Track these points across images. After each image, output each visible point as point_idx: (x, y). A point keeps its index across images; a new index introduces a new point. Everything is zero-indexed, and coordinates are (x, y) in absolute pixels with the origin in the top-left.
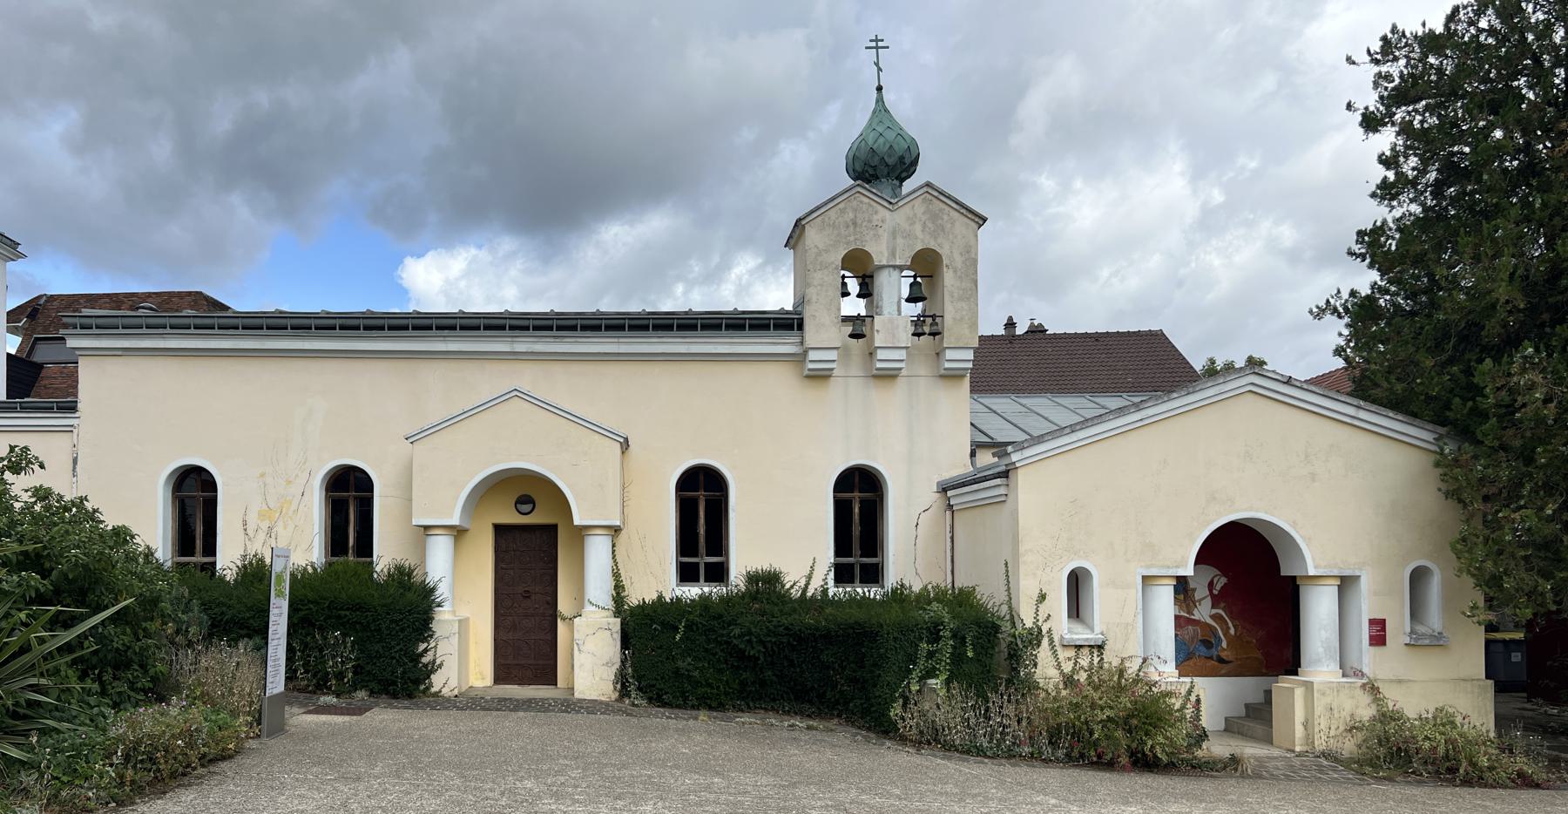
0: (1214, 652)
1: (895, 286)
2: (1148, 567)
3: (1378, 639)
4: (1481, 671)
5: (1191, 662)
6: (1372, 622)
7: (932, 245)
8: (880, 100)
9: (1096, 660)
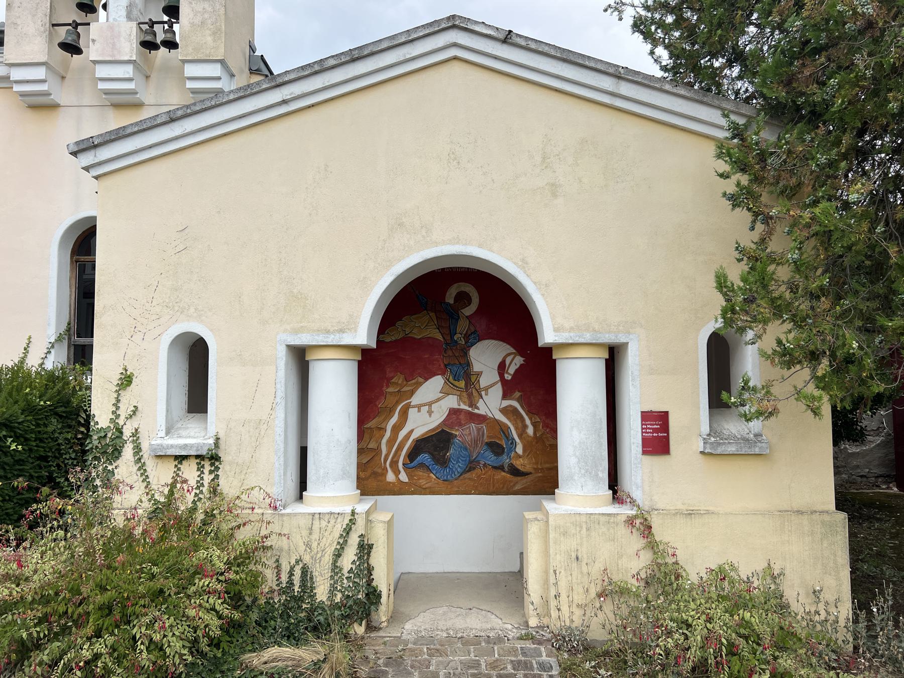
0: (505, 460)
2: (296, 331)
3: (658, 442)
4: (828, 498)
5: (473, 475)
6: (646, 416)
9: (207, 478)
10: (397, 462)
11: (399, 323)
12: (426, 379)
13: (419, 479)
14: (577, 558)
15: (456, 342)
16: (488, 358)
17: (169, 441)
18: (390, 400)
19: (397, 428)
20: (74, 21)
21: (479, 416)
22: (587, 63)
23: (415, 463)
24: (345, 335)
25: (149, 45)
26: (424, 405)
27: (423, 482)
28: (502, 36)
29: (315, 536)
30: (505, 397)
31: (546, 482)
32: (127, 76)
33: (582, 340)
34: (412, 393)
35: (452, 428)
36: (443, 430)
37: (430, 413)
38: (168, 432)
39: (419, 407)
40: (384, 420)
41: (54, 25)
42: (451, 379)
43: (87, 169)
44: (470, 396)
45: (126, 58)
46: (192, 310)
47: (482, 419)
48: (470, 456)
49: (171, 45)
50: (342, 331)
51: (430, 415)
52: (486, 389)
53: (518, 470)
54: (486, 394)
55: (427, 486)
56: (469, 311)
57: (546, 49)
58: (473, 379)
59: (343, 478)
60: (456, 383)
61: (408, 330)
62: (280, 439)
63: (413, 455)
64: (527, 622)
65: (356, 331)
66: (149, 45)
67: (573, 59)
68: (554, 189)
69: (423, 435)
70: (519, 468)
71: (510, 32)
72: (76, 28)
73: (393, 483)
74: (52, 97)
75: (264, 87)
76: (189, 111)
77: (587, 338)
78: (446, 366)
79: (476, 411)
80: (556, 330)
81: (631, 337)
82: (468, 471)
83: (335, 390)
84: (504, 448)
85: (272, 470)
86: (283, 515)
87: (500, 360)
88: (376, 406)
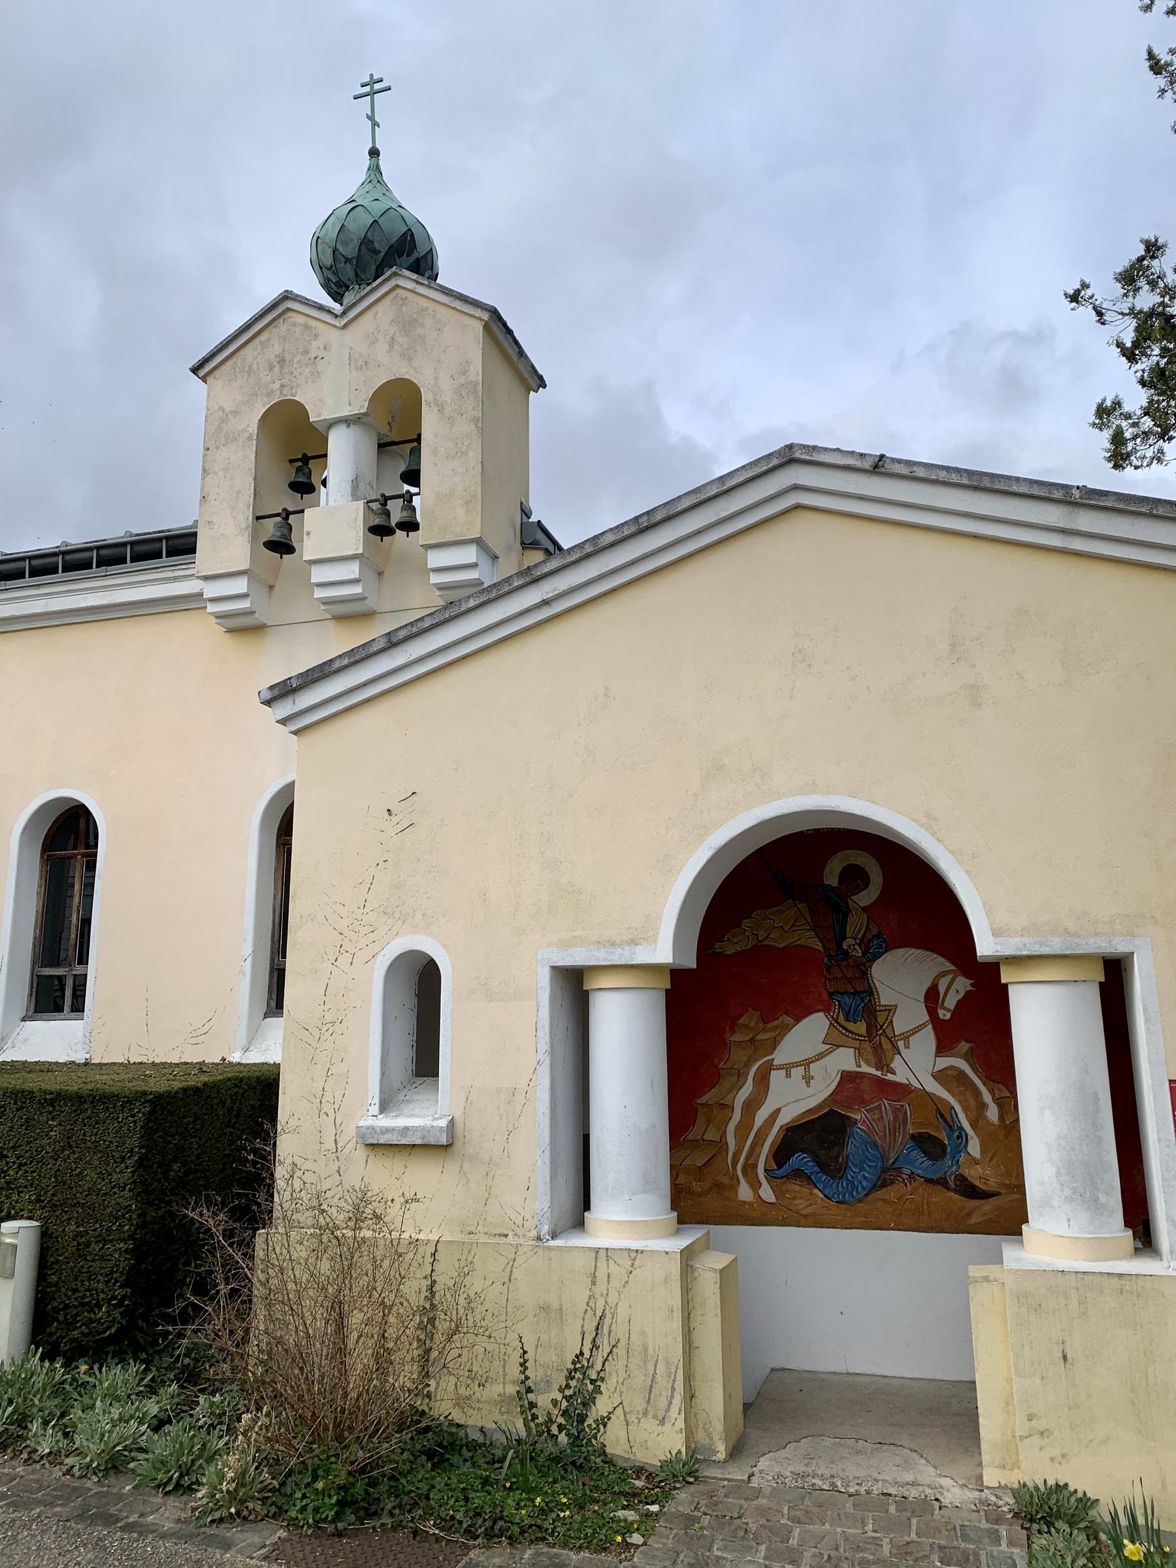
1: (344, 458)
2: (565, 945)
7: (403, 371)
8: (375, 169)
10: (755, 1166)
11: (746, 923)
12: (798, 1020)
13: (794, 1198)
14: (1065, 1358)
15: (846, 953)
16: (903, 981)
17: (385, 1122)
18: (738, 1056)
19: (752, 1106)
20: (285, 510)
21: (896, 1085)
22: (1015, 488)
23: (786, 1168)
24: (638, 948)
25: (381, 531)
26: (796, 1065)
27: (800, 1204)
28: (867, 465)
29: (601, 1288)
30: (942, 1048)
31: (1000, 1210)
32: (352, 576)
33: (1045, 950)
34: (774, 1044)
35: (849, 1108)
36: (831, 1110)
37: (808, 1079)
38: (384, 1107)
39: (788, 1068)
40: (730, 1090)
41: (258, 518)
42: (841, 1019)
43: (283, 722)
44: (878, 1050)
45: (351, 552)
46: (419, 917)
47: (903, 1091)
48: (883, 1158)
49: (410, 526)
50: (634, 942)
51: (808, 1084)
52: (906, 1037)
53: (973, 1187)
54: (907, 1046)
55: (809, 1210)
56: (864, 899)
57: (943, 475)
58: (881, 1017)
59: (644, 1192)
60: (851, 1026)
61: (762, 934)
62: (544, 1121)
63: (781, 1154)
64: (980, 1477)
65: (655, 942)
66: (381, 531)
67: (988, 485)
68: (975, 695)
69: (793, 1121)
70: (977, 1183)
71: (882, 456)
72: (287, 518)
73: (750, 1204)
74: (256, 615)
75: (516, 584)
76: (415, 629)
77: (1055, 945)
78: (831, 995)
79: (890, 1077)
80: (997, 933)
81: (1137, 941)
82: (884, 1185)
83: (627, 1042)
84: (944, 1146)
85: (527, 1174)
86: (549, 1248)
87: (928, 984)
88: (716, 1067)
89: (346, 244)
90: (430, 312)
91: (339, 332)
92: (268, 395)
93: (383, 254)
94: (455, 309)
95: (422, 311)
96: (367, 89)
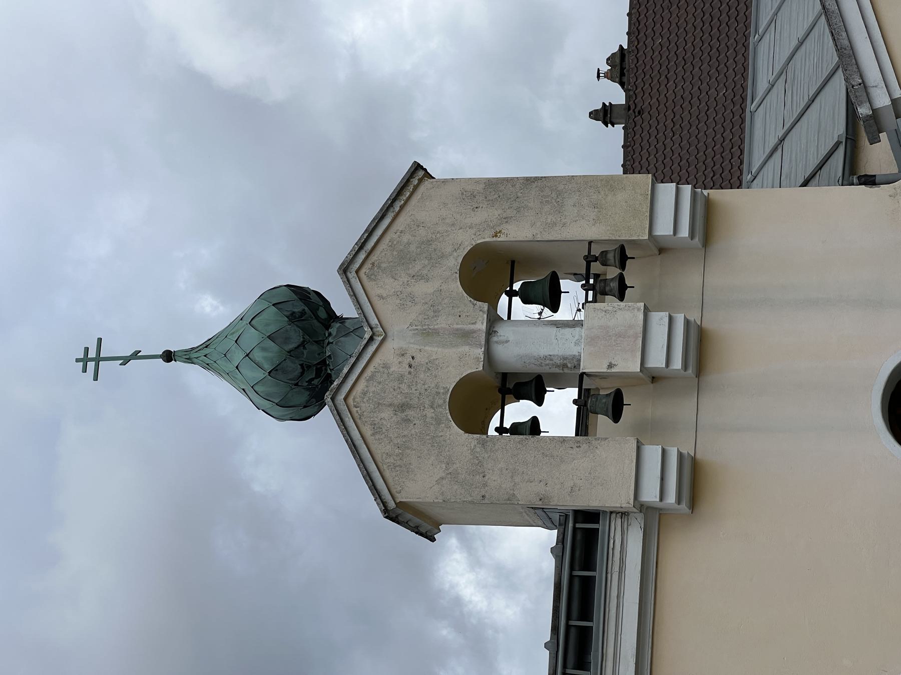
7: (454, 262)
8: (188, 356)
45: (641, 316)
89: (287, 340)
90: (395, 236)
91: (389, 340)
92: (438, 421)
93: (306, 308)
94: (402, 207)
95: (392, 246)
96: (91, 365)
